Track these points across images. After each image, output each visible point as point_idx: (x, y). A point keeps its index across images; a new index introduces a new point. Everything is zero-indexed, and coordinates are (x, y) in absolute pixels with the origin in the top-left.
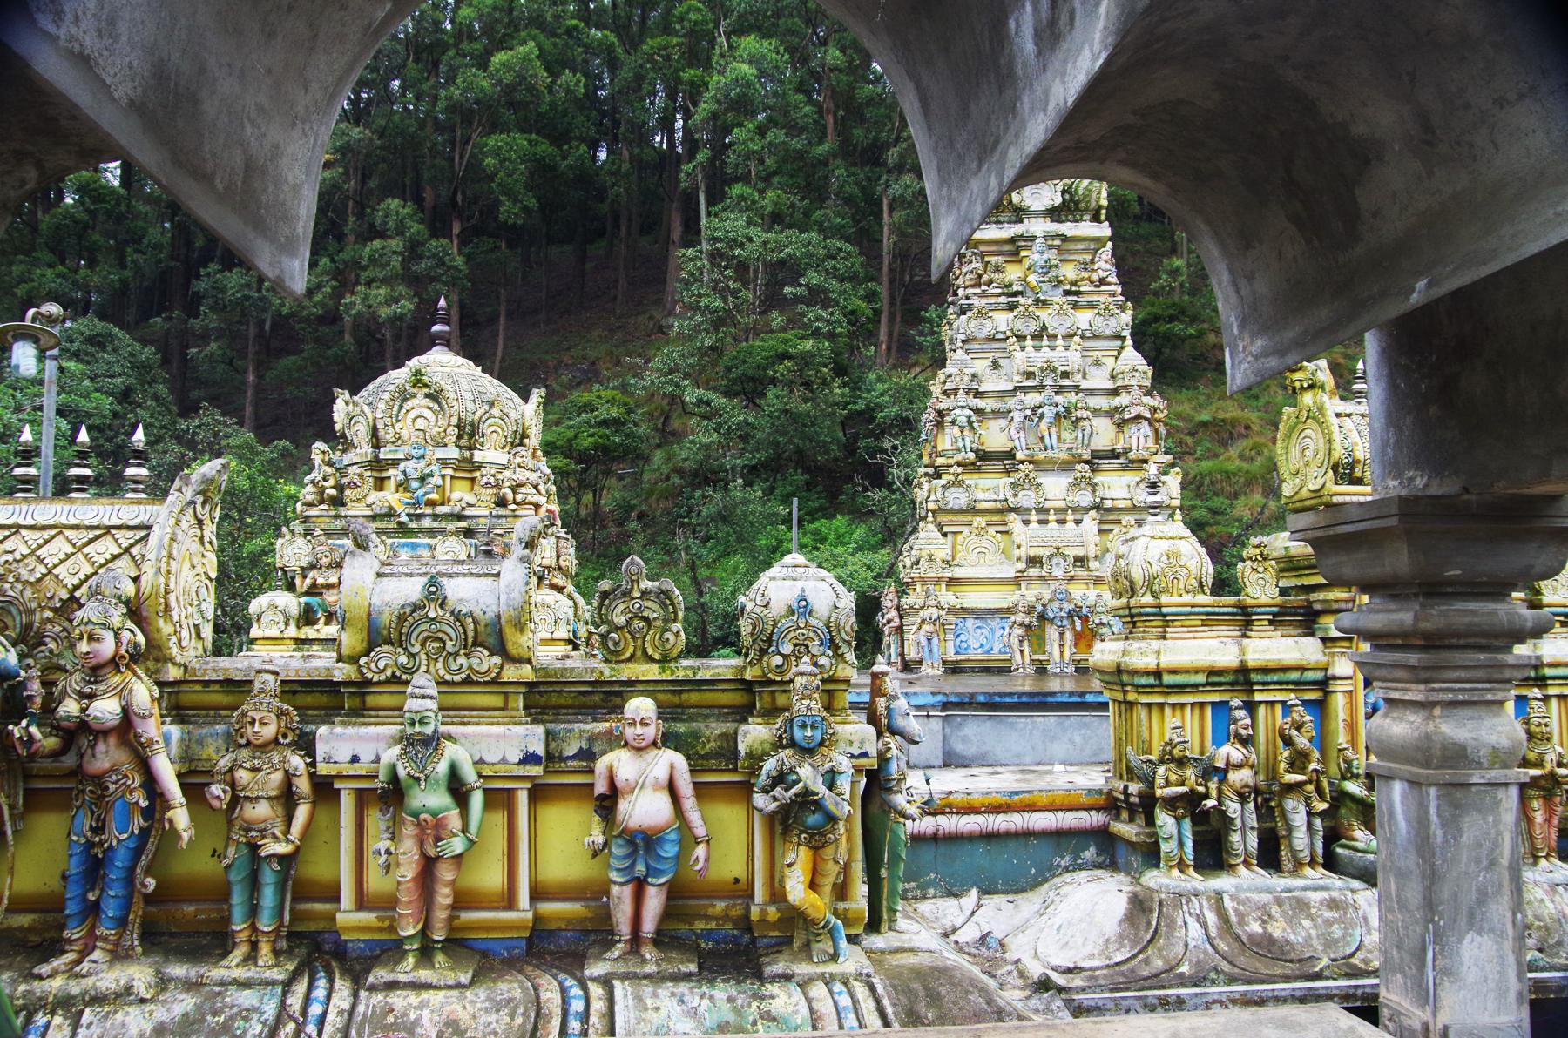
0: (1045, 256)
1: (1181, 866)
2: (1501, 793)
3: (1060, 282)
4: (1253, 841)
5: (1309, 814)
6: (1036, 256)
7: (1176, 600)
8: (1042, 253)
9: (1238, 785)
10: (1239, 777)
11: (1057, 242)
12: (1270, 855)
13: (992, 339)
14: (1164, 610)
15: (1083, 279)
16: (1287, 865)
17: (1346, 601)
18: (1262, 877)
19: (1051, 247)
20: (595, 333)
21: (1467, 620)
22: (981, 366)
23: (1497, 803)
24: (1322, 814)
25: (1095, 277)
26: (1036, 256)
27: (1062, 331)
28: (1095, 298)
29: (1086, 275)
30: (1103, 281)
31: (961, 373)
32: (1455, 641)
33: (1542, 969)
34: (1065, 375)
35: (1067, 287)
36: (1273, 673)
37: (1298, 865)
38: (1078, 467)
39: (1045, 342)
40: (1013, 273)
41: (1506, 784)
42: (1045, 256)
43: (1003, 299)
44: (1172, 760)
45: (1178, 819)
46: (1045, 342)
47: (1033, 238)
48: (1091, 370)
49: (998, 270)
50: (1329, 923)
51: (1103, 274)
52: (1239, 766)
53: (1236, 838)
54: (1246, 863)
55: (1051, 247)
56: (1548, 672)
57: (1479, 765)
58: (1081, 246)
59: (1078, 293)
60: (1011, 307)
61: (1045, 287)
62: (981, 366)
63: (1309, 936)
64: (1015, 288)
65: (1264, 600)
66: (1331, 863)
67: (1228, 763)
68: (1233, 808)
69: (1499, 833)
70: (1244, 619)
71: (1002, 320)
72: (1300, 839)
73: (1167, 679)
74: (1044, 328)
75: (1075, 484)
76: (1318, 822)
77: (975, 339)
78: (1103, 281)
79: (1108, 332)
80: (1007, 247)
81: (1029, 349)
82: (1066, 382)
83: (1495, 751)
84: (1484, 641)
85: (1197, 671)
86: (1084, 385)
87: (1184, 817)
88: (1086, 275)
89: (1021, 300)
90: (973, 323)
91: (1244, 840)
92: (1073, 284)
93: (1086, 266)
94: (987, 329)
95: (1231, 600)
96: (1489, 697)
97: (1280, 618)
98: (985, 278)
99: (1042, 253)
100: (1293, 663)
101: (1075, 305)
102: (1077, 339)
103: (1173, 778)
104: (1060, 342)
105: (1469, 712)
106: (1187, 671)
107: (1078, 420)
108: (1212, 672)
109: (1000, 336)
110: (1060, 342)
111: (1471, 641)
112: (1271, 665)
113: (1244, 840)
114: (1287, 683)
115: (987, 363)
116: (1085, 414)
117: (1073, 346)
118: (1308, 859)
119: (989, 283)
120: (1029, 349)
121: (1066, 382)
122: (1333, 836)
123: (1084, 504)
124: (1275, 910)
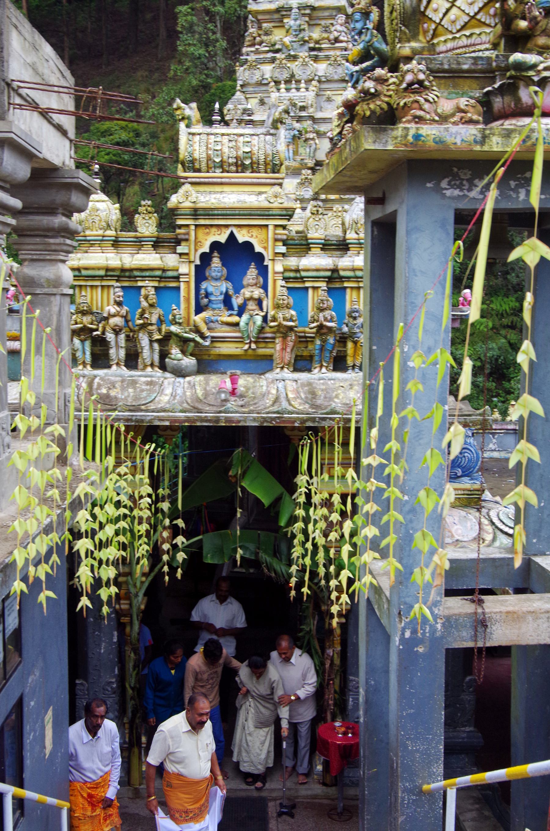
0: (298, 22)
1: (84, 364)
2: (52, 298)
3: (305, 41)
4: (122, 353)
5: (151, 342)
6: (292, 23)
7: (95, 233)
8: (296, 20)
9: (112, 325)
10: (117, 321)
11: (308, 11)
12: (132, 360)
13: (260, 84)
14: (88, 238)
15: (323, 39)
16: (140, 366)
17: (184, 234)
18: (124, 371)
19: (304, 15)
20: (139, 74)
21: (27, 223)
22: (253, 104)
23: (51, 302)
24: (158, 341)
25: (332, 37)
26: (292, 23)
27: (305, 77)
28: (331, 53)
29: (325, 35)
30: (337, 40)
31: (236, 109)
32: (29, 233)
33: (232, 413)
34: (303, 108)
35: (312, 45)
36: (145, 272)
37: (145, 366)
38: (304, 172)
39: (294, 86)
40: (278, 35)
41: (55, 294)
42: (298, 22)
43: (270, 55)
44: (80, 312)
45: (82, 341)
46: (294, 86)
47: (290, 9)
48: (325, 105)
49: (267, 34)
50: (142, 391)
51: (336, 34)
52: (114, 316)
53: (112, 352)
54: (118, 364)
55: (304, 15)
56: (303, 274)
57: (42, 286)
58: (326, 13)
59: (320, 49)
60: (273, 60)
61: (295, 45)
62: (253, 104)
63: (128, 396)
64: (277, 47)
65: (147, 234)
66: (163, 367)
67: (109, 314)
68: (110, 336)
69: (51, 315)
70: (138, 244)
71: (267, 70)
72: (146, 353)
73: (84, 273)
74: (293, 76)
75: (301, 184)
76: (156, 346)
77: (248, 84)
78: (337, 40)
79: (336, 77)
80: (276, 16)
81: (283, 90)
82: (303, 114)
83: (48, 280)
84: (42, 233)
85: (99, 269)
86: (319, 115)
87: (85, 340)
88: (325, 35)
89: (278, 55)
90: (247, 73)
91: (117, 352)
92: (317, 42)
93: (326, 29)
94: (257, 76)
95: (132, 234)
96: (48, 257)
97: (157, 244)
98: (258, 39)
99: (296, 20)
100: (156, 266)
101: (316, 59)
102: (314, 83)
103: (79, 320)
104: (303, 85)
105: (41, 264)
106: (93, 269)
107: (306, 140)
108: (107, 269)
109: (265, 82)
110: (303, 85)
111: (36, 233)
112: (144, 267)
113: (117, 352)
114: (156, 277)
115: (257, 101)
116: (311, 135)
117: (311, 88)
118: (149, 363)
119: (260, 44)
120: (283, 90)
121: (303, 114)
122: (164, 355)
123: (307, 197)
124: (118, 385)
